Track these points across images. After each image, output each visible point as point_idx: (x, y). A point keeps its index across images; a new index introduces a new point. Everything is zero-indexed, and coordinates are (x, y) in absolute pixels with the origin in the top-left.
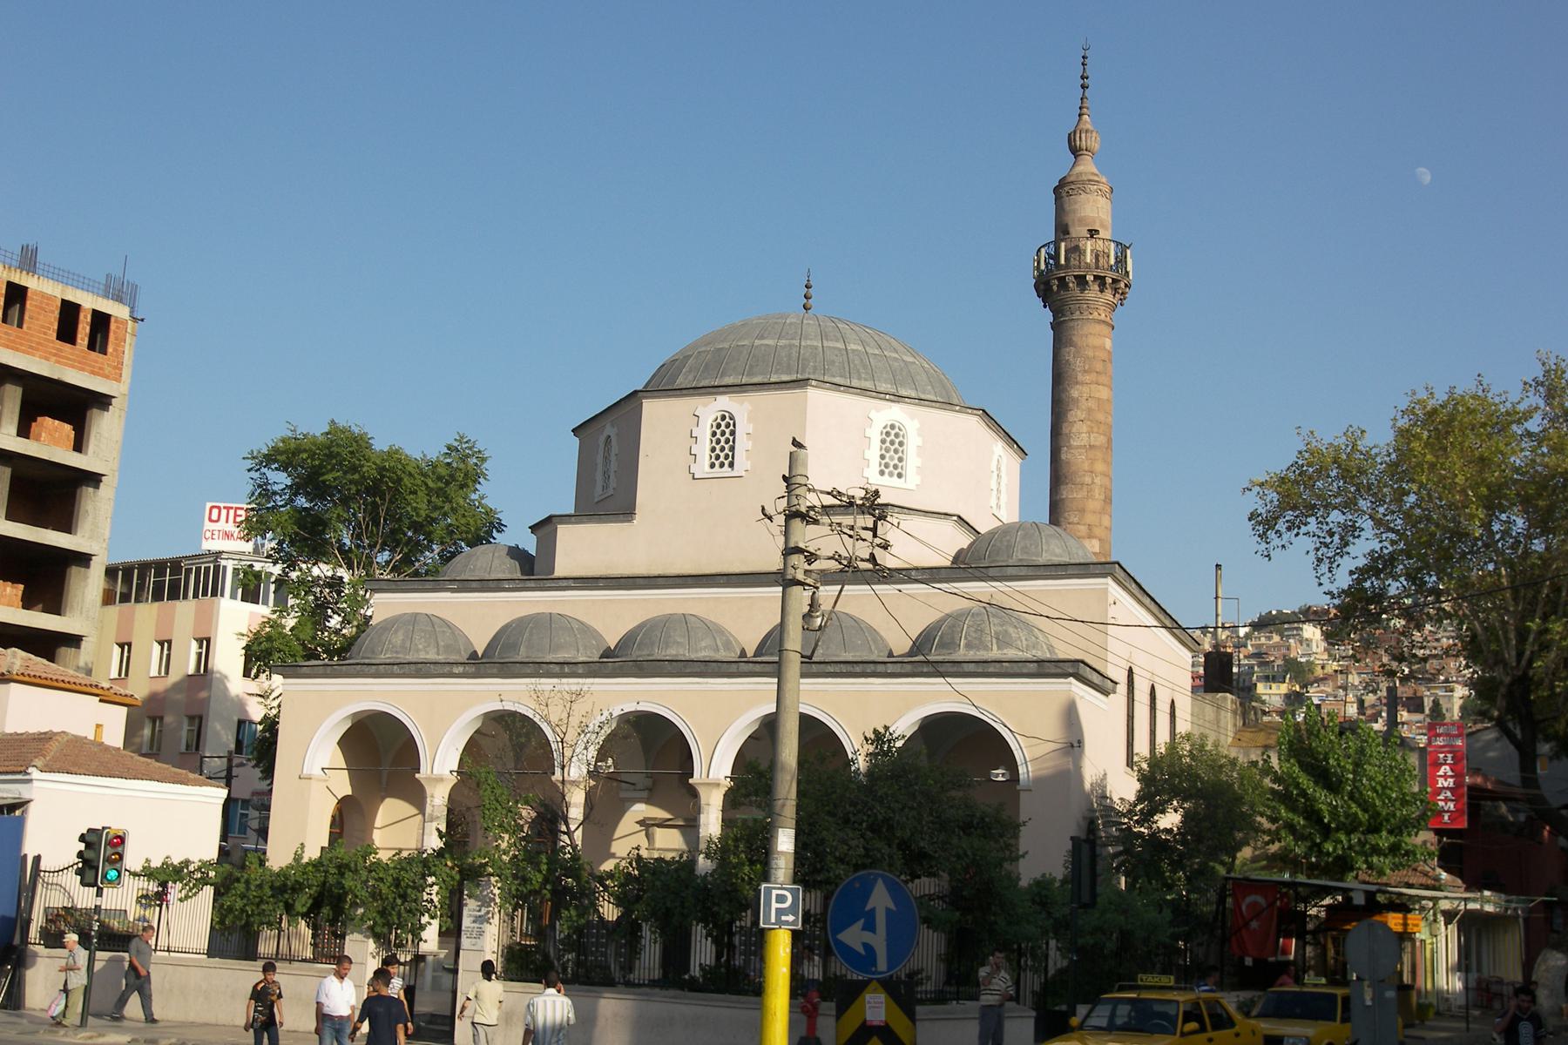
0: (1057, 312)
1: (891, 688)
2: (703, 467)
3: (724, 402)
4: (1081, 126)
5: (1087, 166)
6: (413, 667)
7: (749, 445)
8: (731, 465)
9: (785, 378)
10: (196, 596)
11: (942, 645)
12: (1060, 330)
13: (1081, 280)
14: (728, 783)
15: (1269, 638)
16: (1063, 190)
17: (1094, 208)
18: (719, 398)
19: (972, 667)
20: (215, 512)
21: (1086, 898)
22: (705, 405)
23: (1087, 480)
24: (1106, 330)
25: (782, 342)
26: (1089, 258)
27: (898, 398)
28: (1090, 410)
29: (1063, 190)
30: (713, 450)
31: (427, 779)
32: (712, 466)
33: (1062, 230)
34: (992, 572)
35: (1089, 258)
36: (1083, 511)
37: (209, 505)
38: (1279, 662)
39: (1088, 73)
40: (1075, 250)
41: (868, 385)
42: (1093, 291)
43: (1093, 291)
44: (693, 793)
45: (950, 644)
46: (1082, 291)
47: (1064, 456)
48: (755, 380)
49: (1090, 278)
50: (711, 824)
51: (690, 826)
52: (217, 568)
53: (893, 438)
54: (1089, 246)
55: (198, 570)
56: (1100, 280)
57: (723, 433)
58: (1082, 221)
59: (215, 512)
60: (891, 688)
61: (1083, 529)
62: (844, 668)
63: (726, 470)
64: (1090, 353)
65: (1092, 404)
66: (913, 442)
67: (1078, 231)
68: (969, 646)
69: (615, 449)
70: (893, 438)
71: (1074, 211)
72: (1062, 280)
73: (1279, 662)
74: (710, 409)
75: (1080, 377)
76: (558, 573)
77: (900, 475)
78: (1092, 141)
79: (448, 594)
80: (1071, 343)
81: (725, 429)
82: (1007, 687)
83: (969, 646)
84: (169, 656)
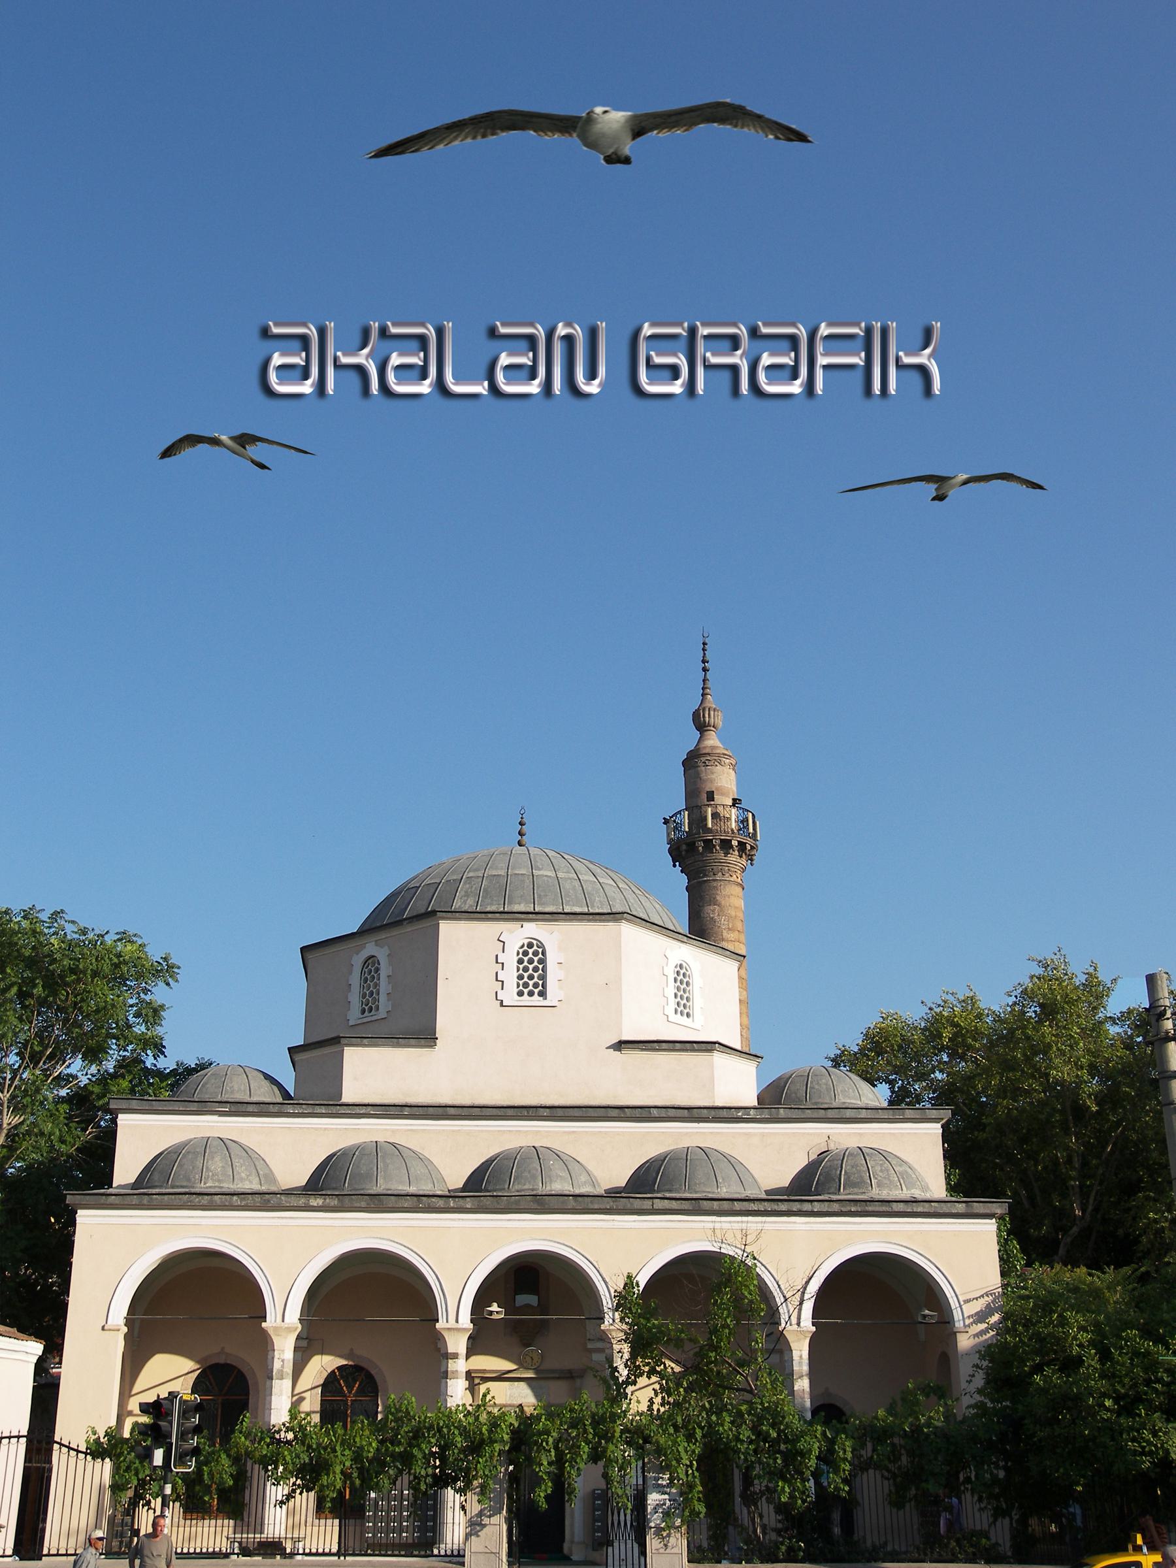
1: (815, 1227)
2: (510, 995)
4: (707, 705)
5: (712, 741)
6: (258, 1198)
7: (561, 974)
8: (542, 994)
9: (578, 910)
16: (694, 762)
17: (724, 780)
18: (526, 924)
19: (900, 1207)
22: (511, 932)
24: (738, 890)
29: (694, 762)
30: (520, 977)
31: (276, 1329)
32: (520, 994)
34: (210, 1107)
39: (708, 658)
42: (734, 857)
43: (734, 857)
46: (726, 854)
48: (547, 910)
57: (531, 961)
60: (815, 1227)
62: (726, 1205)
63: (536, 1000)
66: (697, 982)
71: (712, 781)
74: (518, 934)
75: (725, 934)
76: (346, 1099)
77: (688, 1015)
78: (718, 719)
79: (215, 1118)
81: (533, 961)
82: (933, 1227)
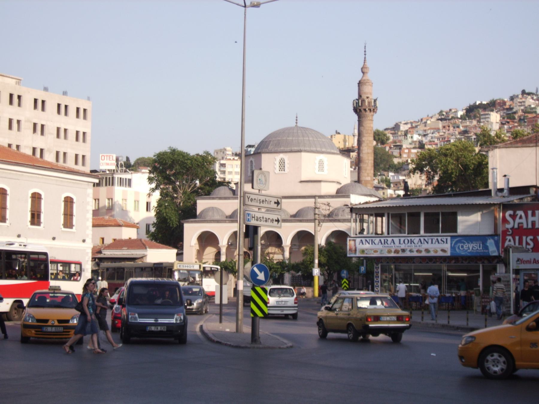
0: (360, 117)
3: (282, 156)
10: (106, 185)
11: (336, 215)
12: (360, 123)
13: (365, 110)
14: (290, 246)
15: (471, 122)
20: (103, 157)
21: (137, 202)
23: (367, 161)
25: (294, 138)
26: (367, 104)
27: (322, 153)
28: (367, 144)
33: (360, 96)
35: (367, 104)
36: (366, 170)
37: (101, 155)
38: (474, 137)
40: (363, 101)
41: (314, 149)
43: (368, 113)
44: (283, 248)
45: (337, 215)
47: (361, 155)
49: (367, 109)
50: (287, 254)
51: (283, 255)
52: (113, 178)
53: (321, 163)
54: (367, 101)
55: (106, 178)
56: (370, 110)
58: (365, 93)
59: (103, 157)
61: (366, 174)
64: (367, 128)
65: (368, 142)
67: (364, 97)
68: (341, 216)
69: (254, 164)
70: (321, 163)
72: (360, 110)
73: (474, 137)
74: (279, 157)
75: (365, 135)
80: (363, 126)
83: (341, 216)
84: (98, 203)
